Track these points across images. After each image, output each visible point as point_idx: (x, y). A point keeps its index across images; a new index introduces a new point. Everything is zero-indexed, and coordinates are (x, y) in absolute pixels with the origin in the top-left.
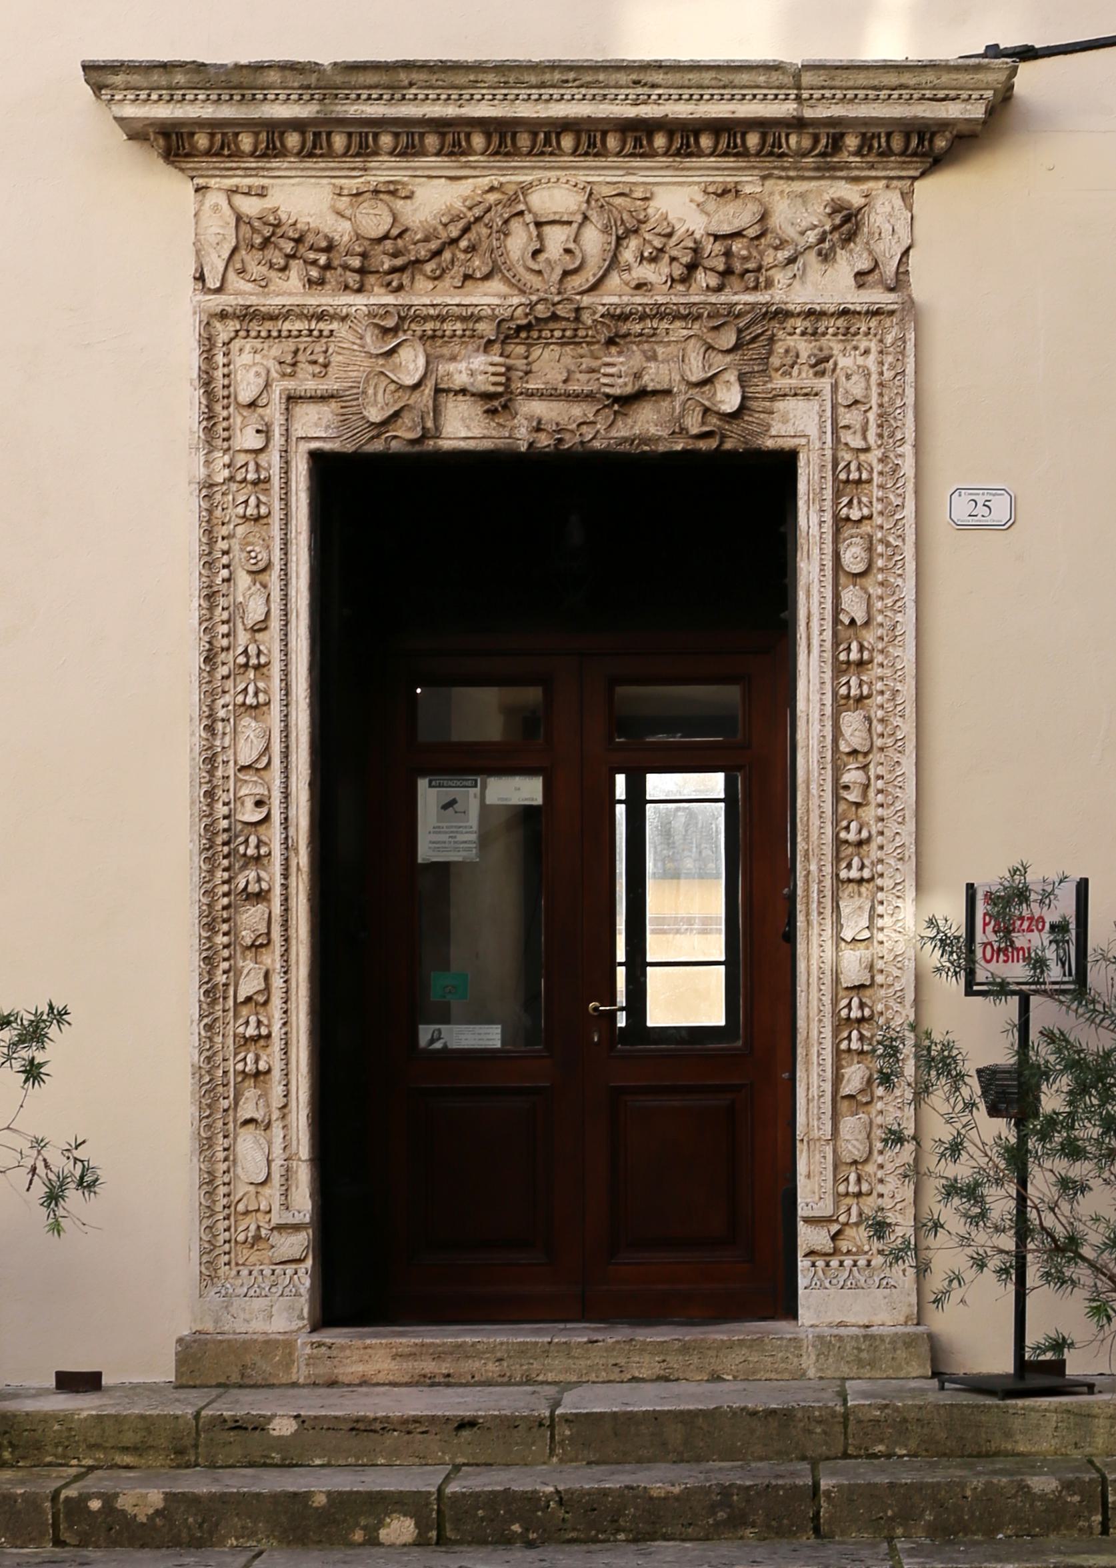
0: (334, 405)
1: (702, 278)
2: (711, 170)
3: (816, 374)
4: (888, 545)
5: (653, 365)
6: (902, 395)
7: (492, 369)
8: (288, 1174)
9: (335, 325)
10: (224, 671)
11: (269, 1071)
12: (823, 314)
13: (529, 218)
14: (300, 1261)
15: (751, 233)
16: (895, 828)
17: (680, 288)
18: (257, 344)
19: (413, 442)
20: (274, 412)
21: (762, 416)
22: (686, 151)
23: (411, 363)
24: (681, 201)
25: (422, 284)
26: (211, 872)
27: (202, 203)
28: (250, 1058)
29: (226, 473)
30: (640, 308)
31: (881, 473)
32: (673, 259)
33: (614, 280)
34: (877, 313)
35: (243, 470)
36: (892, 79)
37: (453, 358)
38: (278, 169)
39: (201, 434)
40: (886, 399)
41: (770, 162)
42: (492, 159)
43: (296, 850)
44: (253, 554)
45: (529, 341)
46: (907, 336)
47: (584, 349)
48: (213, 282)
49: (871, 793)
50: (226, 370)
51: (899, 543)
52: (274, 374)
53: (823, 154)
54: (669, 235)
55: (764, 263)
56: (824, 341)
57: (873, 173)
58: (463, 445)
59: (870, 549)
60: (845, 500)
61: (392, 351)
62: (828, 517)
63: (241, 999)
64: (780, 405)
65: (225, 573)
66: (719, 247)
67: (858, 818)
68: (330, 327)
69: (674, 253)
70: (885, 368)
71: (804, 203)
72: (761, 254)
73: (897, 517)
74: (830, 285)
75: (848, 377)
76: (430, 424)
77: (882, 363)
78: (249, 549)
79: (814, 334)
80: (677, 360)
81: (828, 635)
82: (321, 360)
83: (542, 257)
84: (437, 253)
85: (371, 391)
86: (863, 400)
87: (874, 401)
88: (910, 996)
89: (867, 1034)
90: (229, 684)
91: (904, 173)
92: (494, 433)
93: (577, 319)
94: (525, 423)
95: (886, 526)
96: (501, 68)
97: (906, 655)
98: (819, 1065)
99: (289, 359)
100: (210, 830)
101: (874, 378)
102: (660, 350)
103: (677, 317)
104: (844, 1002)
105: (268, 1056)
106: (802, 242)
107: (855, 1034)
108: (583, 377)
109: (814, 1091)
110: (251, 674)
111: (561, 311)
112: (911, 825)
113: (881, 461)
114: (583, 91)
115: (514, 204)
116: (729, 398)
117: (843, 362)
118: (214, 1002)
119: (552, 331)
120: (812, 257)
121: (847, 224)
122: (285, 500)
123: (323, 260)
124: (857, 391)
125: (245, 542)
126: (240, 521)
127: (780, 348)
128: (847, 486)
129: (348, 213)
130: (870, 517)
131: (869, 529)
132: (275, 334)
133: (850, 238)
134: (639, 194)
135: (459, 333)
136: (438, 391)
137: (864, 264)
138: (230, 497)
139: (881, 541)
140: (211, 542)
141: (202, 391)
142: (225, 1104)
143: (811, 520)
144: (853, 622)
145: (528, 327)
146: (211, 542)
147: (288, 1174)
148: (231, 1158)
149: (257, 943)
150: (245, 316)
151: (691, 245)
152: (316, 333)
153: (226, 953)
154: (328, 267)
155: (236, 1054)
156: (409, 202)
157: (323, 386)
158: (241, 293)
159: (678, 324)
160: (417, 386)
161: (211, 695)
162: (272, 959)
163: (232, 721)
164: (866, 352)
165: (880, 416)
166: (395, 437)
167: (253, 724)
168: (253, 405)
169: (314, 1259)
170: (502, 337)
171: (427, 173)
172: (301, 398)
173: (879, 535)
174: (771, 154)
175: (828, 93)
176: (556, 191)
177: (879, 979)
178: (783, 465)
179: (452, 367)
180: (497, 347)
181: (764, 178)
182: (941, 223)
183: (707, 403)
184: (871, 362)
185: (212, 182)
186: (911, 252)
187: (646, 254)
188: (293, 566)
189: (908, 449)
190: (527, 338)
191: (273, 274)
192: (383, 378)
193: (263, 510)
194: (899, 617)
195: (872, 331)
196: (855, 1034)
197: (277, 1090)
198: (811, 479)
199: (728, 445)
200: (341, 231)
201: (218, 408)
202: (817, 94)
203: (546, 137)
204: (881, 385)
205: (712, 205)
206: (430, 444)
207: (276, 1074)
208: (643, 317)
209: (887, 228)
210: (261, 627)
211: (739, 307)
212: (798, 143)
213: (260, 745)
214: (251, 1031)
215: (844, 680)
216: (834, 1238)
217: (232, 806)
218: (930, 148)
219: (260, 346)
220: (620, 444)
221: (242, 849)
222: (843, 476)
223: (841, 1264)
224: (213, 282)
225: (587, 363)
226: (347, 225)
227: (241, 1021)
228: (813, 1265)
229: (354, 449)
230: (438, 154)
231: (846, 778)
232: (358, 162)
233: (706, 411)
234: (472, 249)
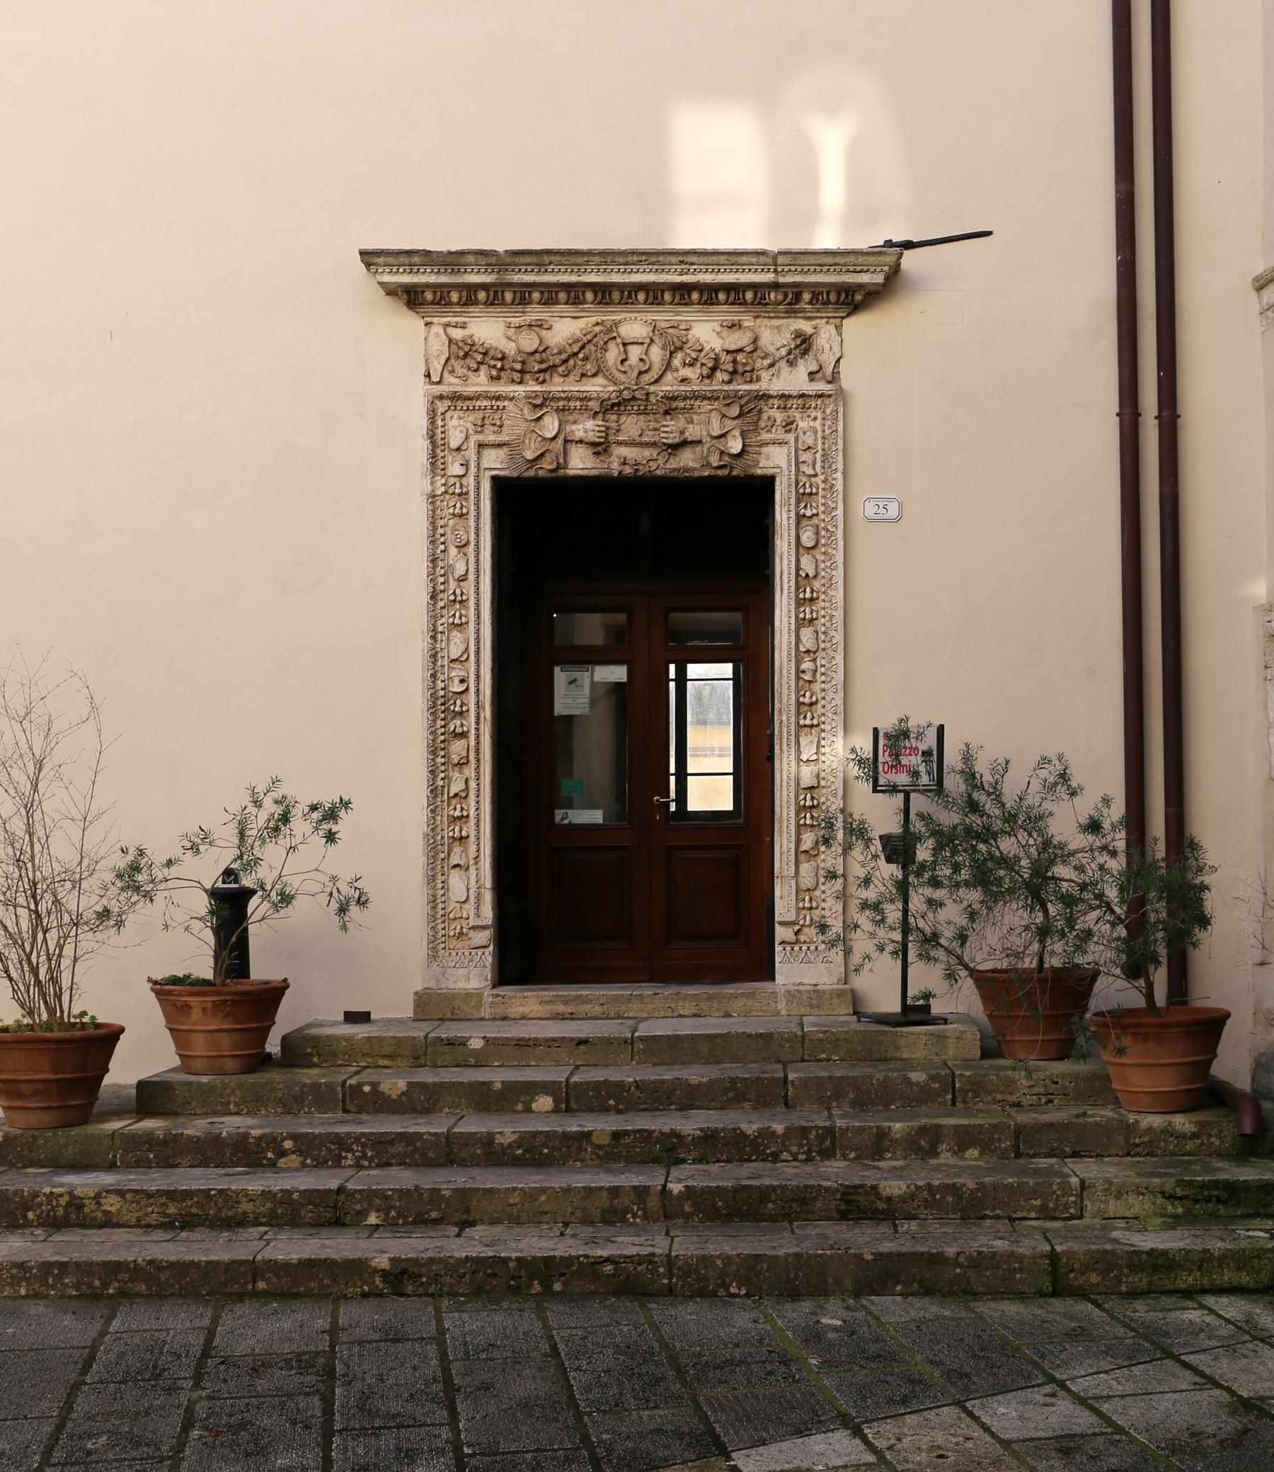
2: (726, 313)
4: (827, 530)
12: (790, 396)
19: (551, 471)
20: (471, 454)
22: (712, 301)
23: (551, 425)
24: (707, 331)
32: (703, 365)
33: (669, 377)
34: (821, 396)
41: (759, 308)
56: (790, 412)
58: (580, 472)
59: (817, 533)
61: (540, 418)
62: (793, 514)
64: (765, 449)
65: (442, 547)
69: (703, 361)
83: (626, 364)
84: (566, 361)
87: (819, 448)
93: (647, 399)
101: (820, 433)
106: (778, 355)
108: (650, 433)
111: (638, 395)
116: (735, 446)
117: (801, 424)
121: (804, 344)
123: (499, 365)
124: (810, 442)
125: (454, 529)
127: (764, 416)
133: (806, 352)
136: (566, 441)
137: (814, 368)
143: (783, 516)
145: (619, 404)
154: (502, 369)
164: (815, 419)
168: (458, 449)
175: (793, 268)
178: (767, 483)
181: (756, 317)
182: (858, 342)
185: (435, 320)
188: (482, 543)
189: (839, 475)
198: (782, 492)
199: (735, 473)
201: (438, 451)
202: (786, 269)
203: (629, 294)
204: (823, 438)
218: (852, 300)
226: (513, 345)
230: (566, 303)
233: (722, 453)
234: (586, 359)
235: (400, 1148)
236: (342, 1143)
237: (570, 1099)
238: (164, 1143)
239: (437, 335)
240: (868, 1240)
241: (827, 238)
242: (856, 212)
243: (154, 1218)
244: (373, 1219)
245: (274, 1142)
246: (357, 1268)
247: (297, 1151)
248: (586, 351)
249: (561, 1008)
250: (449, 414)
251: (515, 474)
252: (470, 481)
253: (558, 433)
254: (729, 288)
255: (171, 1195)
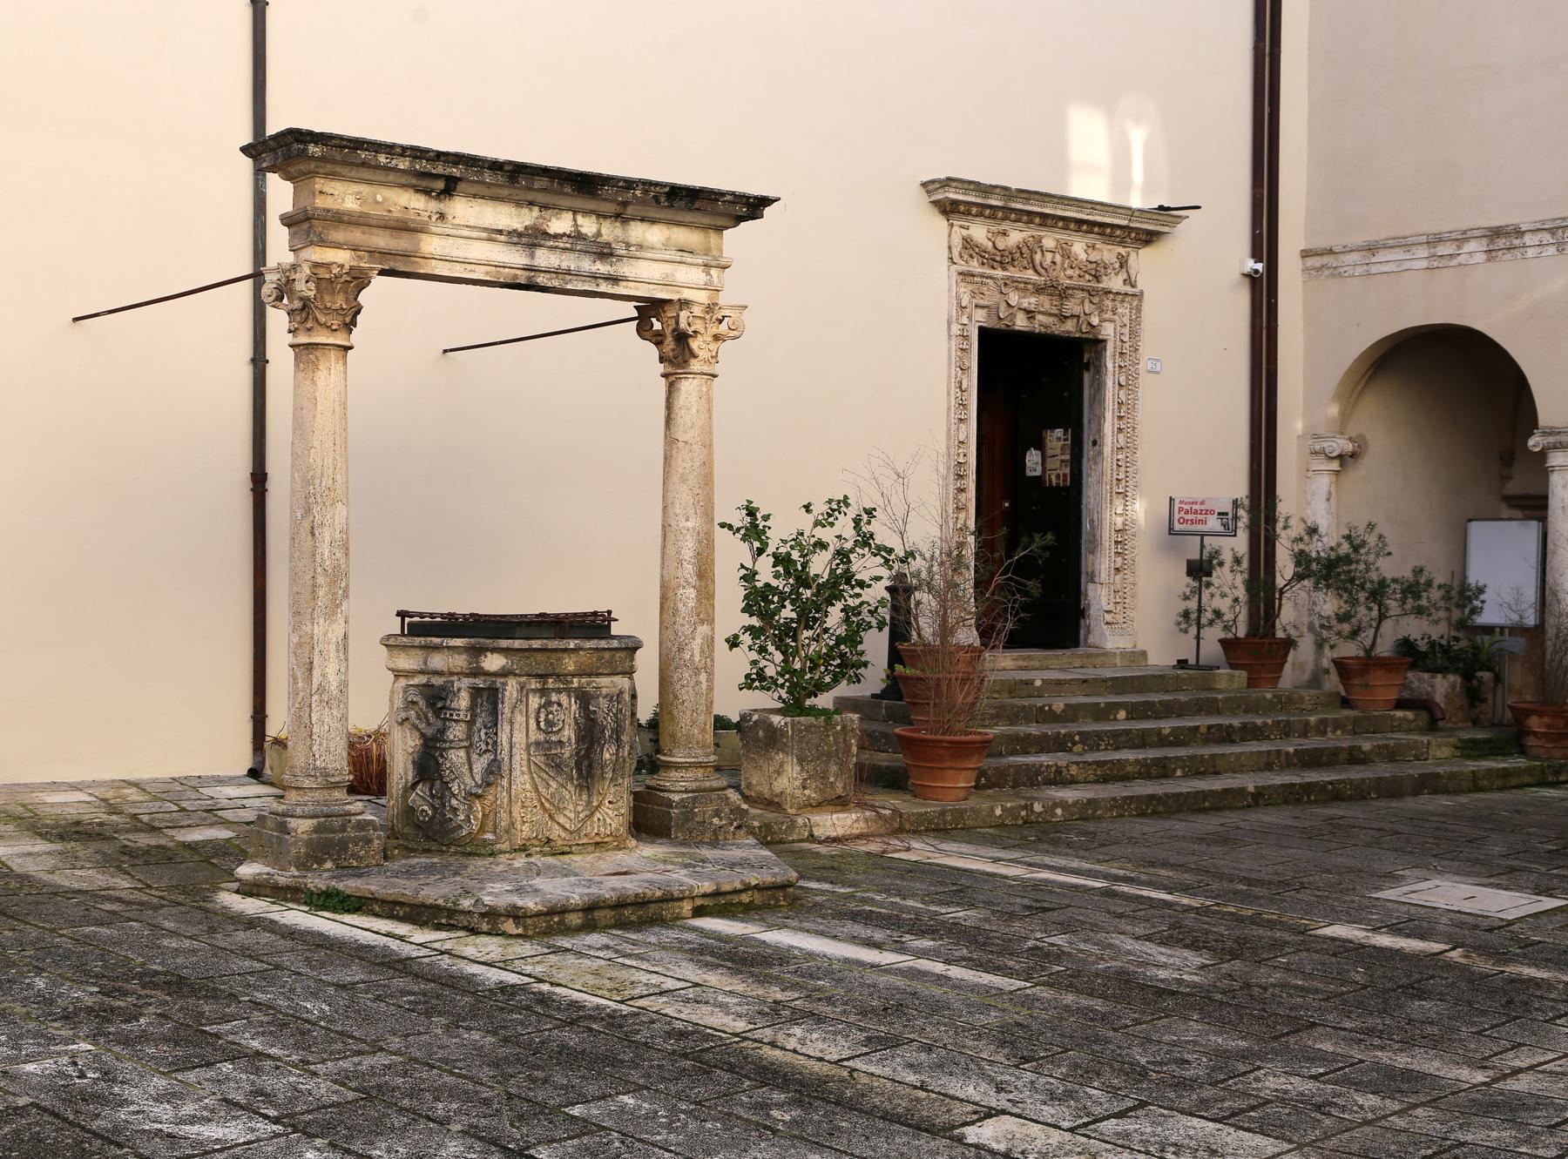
2: (1090, 239)
96: (496, 166)
121: (1123, 262)
182: (1144, 261)
203: (1046, 220)
218: (1149, 238)
235: (1123, 738)
236: (1099, 735)
237: (1135, 712)
238: (1023, 740)
240: (1356, 774)
241: (1136, 202)
242: (1148, 188)
243: (1092, 777)
244: (1179, 773)
245: (1070, 736)
246: (1242, 791)
247: (1081, 742)
249: (1021, 663)
254: (1080, 222)
255: (1099, 763)
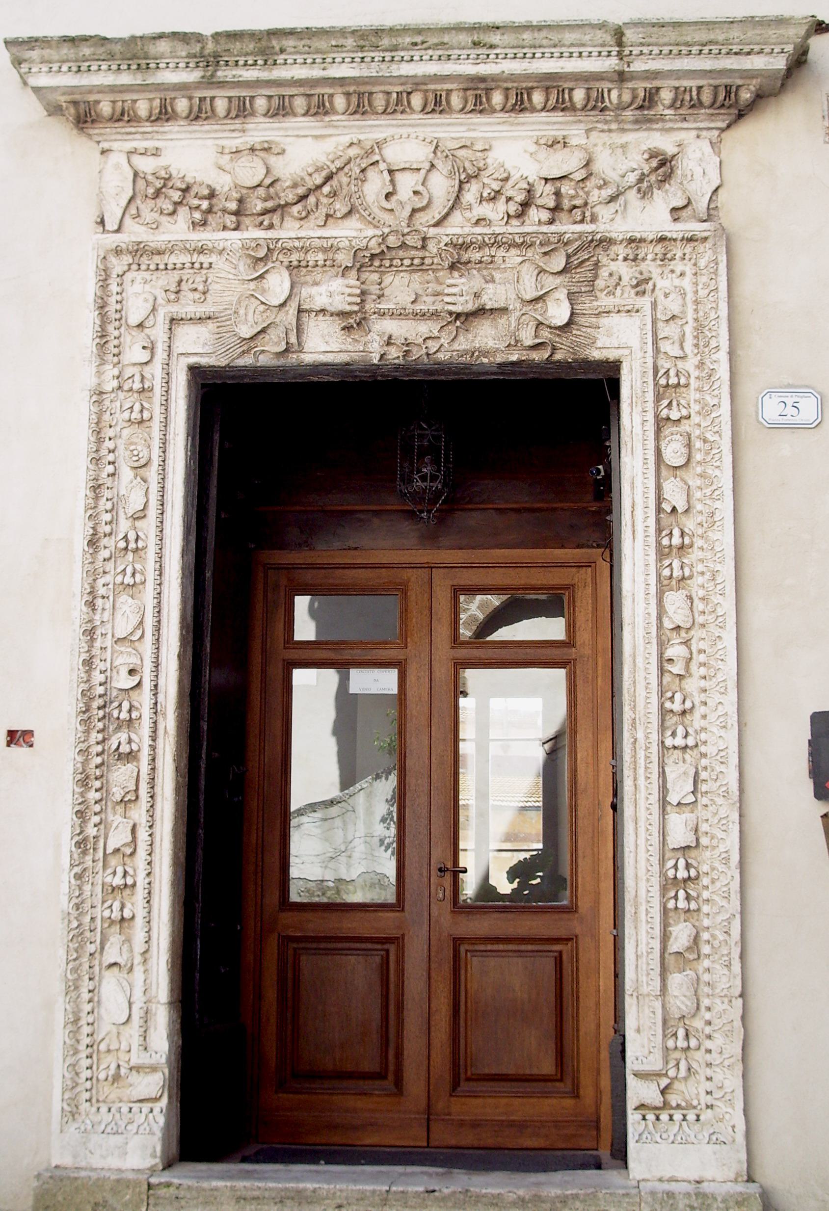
0: (211, 325)
1: (534, 214)
3: (637, 294)
4: (705, 441)
5: (491, 285)
6: (716, 309)
7: (349, 291)
8: (147, 1016)
9: (213, 258)
10: (105, 554)
11: (133, 917)
12: (642, 240)
13: (382, 166)
14: (157, 1099)
15: (578, 176)
16: (717, 698)
17: (514, 222)
18: (147, 275)
20: (159, 332)
21: (589, 330)
23: (278, 284)
24: (517, 149)
25: (289, 223)
26: (87, 732)
27: (105, 163)
28: (116, 905)
29: (115, 384)
30: (480, 238)
31: (697, 378)
32: (509, 199)
33: (457, 217)
34: (691, 240)
35: (131, 380)
36: (703, 36)
37: (316, 284)
38: (171, 132)
39: (94, 349)
40: (701, 314)
42: (352, 117)
43: (164, 715)
44: (135, 453)
45: (382, 269)
46: (719, 259)
47: (431, 276)
48: (111, 225)
49: (694, 666)
50: (119, 298)
51: (716, 437)
52: (160, 301)
53: (641, 107)
54: (506, 179)
55: (590, 201)
56: (643, 266)
57: (685, 125)
60: (665, 402)
61: (261, 277)
62: (650, 417)
63: (109, 850)
64: (604, 321)
65: (110, 469)
66: (550, 188)
67: (682, 690)
68: (210, 260)
69: (510, 193)
70: (699, 288)
71: (624, 153)
72: (588, 194)
73: (714, 415)
74: (651, 217)
75: (666, 295)
76: (293, 340)
77: (696, 284)
78: (132, 448)
79: (635, 260)
80: (511, 282)
81: (652, 522)
82: (201, 288)
83: (394, 199)
84: (303, 198)
85: (242, 312)
86: (680, 315)
88: (735, 857)
89: (693, 893)
90: (109, 566)
91: (712, 125)
92: (350, 348)
94: (378, 338)
95: (703, 424)
97: (725, 538)
98: (648, 922)
99: (173, 288)
100: (87, 695)
101: (690, 297)
102: (497, 276)
103: (514, 245)
104: (671, 863)
105: (132, 904)
107: (681, 894)
108: (429, 299)
109: (643, 948)
110: (130, 556)
111: (410, 241)
112: (733, 695)
113: (698, 367)
114: (430, 52)
115: (370, 157)
116: (558, 312)
118: (85, 853)
119: (402, 260)
120: (632, 195)
121: (664, 166)
122: (166, 405)
123: (205, 205)
124: (675, 309)
126: (126, 425)
127: (604, 273)
128: (665, 390)
129: (228, 167)
130: (688, 417)
131: (688, 429)
132: (162, 267)
133: (666, 178)
134: (479, 146)
135: (321, 263)
136: (300, 311)
138: (118, 404)
139: (699, 437)
140: (100, 441)
141: (97, 312)
142: (91, 948)
144: (674, 509)
146: (100, 441)
147: (147, 1016)
148: (96, 999)
149: (126, 799)
150: (137, 251)
151: (526, 186)
152: (197, 265)
153: (97, 808)
154: (209, 211)
155: (103, 902)
156: (280, 156)
157: (201, 310)
158: (135, 232)
159: (513, 251)
160: (283, 305)
161: (93, 575)
162: (139, 813)
163: (111, 598)
164: (682, 274)
165: (696, 329)
166: (263, 351)
167: (130, 600)
168: (140, 326)
169: (170, 1097)
170: (358, 265)
171: (296, 133)
172: (182, 319)
173: (697, 432)
174: (594, 108)
175: (645, 50)
176: (407, 141)
177: (704, 841)
179: (314, 290)
180: (353, 273)
181: (588, 131)
183: (539, 318)
184: (687, 283)
185: (115, 145)
186: (720, 191)
187: (485, 195)
188: (169, 462)
189: (723, 356)
190: (381, 266)
191: (164, 219)
192: (253, 300)
193: (146, 415)
194: (717, 504)
195: (687, 257)
196: (681, 894)
197: (139, 936)
199: (558, 356)
200: (222, 183)
201: (110, 328)
204: (696, 302)
205: (543, 153)
206: (293, 359)
207: (139, 922)
208: (482, 246)
209: (698, 171)
210: (140, 516)
211: (567, 236)
212: (620, 96)
213: (134, 620)
214: (118, 881)
215: (667, 562)
216: (663, 1092)
217: (108, 674)
219: (149, 278)
220: (462, 356)
221: (115, 714)
222: (663, 382)
223: (671, 1118)
224: (111, 225)
225: (433, 287)
227: (109, 871)
228: (644, 1118)
229: (227, 362)
230: (306, 114)
231: (670, 653)
232: (237, 124)
234: (334, 194)
239: (117, 166)
248: (334, 182)
250: (129, 276)
251: (223, 362)
252: (156, 371)
253: (290, 297)
